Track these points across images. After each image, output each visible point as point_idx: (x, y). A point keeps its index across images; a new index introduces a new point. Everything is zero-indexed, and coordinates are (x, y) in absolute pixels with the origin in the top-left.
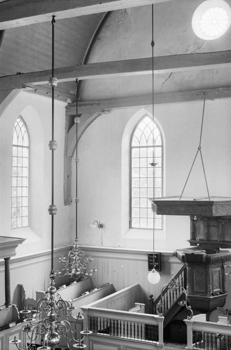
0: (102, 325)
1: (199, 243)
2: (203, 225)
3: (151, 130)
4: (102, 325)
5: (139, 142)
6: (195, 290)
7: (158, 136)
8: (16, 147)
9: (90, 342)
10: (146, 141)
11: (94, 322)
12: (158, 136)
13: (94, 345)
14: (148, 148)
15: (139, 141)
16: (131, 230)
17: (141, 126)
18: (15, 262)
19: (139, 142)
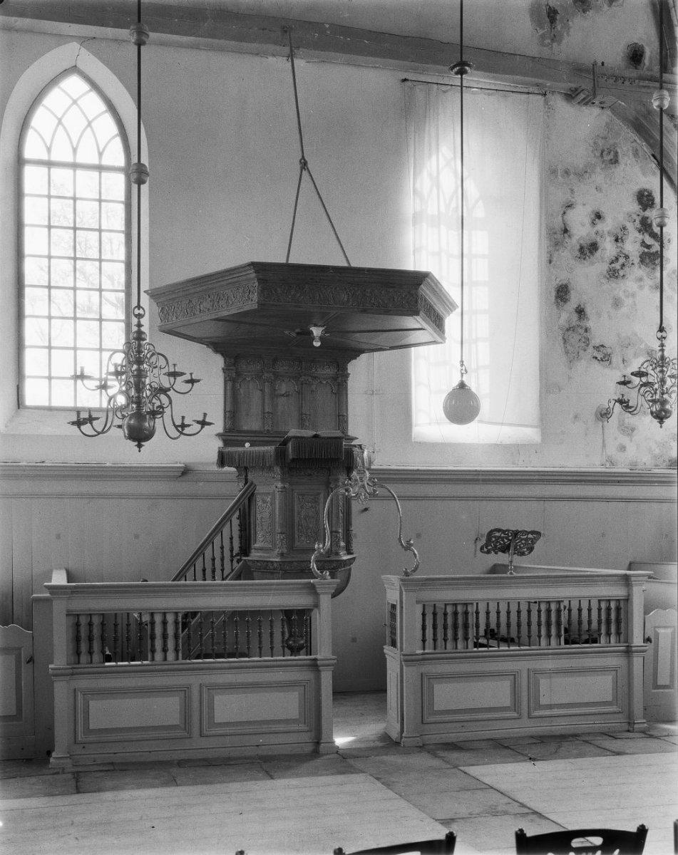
0: (266, 637)
1: (248, 441)
2: (259, 393)
3: (55, 116)
4: (266, 637)
5: (75, 150)
6: (297, 544)
7: (55, 131)
8: (69, 172)
9: (75, 697)
10: (71, 151)
11: (91, 647)
12: (55, 131)
13: (93, 704)
14: (104, 174)
15: (101, 150)
16: (22, 412)
17: (54, 99)
18: (609, 481)
19: (75, 150)
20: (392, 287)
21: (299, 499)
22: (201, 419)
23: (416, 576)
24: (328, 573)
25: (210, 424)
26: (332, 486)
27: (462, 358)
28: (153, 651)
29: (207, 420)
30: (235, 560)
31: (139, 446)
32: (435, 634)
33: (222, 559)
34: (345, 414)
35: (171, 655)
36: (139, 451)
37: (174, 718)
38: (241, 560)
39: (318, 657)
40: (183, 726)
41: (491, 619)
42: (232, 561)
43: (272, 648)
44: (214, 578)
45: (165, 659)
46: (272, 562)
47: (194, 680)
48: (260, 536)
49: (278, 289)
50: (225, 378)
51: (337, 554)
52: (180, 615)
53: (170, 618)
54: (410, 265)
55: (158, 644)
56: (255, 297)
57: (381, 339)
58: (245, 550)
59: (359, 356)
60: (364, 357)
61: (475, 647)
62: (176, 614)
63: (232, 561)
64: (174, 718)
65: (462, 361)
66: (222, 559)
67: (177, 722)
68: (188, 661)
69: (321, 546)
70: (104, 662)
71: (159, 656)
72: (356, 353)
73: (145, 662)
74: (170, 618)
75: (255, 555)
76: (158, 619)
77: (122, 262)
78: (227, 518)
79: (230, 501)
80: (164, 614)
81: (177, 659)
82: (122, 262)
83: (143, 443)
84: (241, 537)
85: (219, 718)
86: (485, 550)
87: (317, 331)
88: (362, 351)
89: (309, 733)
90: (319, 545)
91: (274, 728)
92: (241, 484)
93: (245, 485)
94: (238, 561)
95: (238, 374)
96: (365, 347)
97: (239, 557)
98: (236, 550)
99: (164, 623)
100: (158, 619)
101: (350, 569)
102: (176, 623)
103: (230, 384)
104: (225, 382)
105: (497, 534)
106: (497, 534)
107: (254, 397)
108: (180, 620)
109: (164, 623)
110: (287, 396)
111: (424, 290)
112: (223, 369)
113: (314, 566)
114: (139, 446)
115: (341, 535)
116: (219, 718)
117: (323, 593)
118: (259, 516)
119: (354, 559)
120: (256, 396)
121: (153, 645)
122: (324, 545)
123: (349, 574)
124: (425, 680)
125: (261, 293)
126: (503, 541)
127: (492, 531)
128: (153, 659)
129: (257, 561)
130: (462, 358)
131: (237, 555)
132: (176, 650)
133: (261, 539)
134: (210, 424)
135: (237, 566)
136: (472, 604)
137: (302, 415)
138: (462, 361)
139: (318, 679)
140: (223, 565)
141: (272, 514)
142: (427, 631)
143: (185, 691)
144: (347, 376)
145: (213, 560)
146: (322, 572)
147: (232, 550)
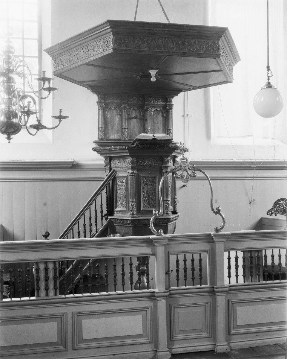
20: (202, 39)
21: (143, 180)
22: (58, 114)
23: (222, 232)
24: (162, 231)
25: (65, 117)
26: (164, 171)
27: (268, 64)
28: (38, 290)
29: (63, 114)
30: (104, 219)
31: (9, 138)
32: (237, 273)
33: (96, 218)
34: (171, 129)
35: (51, 293)
36: (9, 142)
37: (54, 337)
38: (108, 218)
39: (156, 290)
40: (60, 343)
41: (275, 261)
42: (102, 219)
43: (123, 285)
44: (85, 237)
45: (47, 295)
46: (127, 220)
47: (69, 310)
48: (119, 203)
49: (126, 40)
50: (98, 107)
51: (167, 214)
52: (57, 263)
53: (51, 266)
54: (212, 22)
55: (51, 275)
56: (111, 46)
57: (194, 80)
58: (111, 211)
59: (179, 93)
60: (181, 94)
61: (264, 280)
62: (54, 262)
63: (102, 219)
64: (54, 337)
65: (268, 67)
66: (96, 218)
67: (56, 340)
68: (63, 296)
69: (157, 212)
70: (2, 299)
71: (43, 293)
72: (177, 91)
73: (32, 298)
74: (51, 266)
75: (116, 216)
76: (42, 267)
77: (36, 39)
78: (99, 192)
79: (100, 182)
80: (46, 263)
81: (56, 294)
82: (36, 39)
83: (12, 136)
84: (107, 204)
85: (85, 336)
86: (270, 213)
87: (153, 73)
88: (181, 91)
89: (150, 345)
90: (155, 211)
91: (126, 341)
92: (108, 171)
93: (110, 171)
94: (106, 219)
95: (107, 105)
96: (181, 87)
97: (106, 217)
98: (105, 212)
99: (46, 269)
100: (42, 267)
101: (176, 222)
102: (55, 269)
103: (101, 112)
104: (99, 110)
105: (281, 202)
106: (281, 202)
107: (115, 117)
108: (58, 267)
109: (46, 269)
110: (136, 118)
111: (227, 31)
112: (97, 102)
113: (152, 227)
114: (9, 138)
115: (170, 202)
116: (85, 336)
117: (159, 246)
118: (119, 192)
119: (178, 216)
120: (117, 118)
121: (38, 286)
122: (159, 212)
123: (175, 226)
124: (231, 304)
125: (115, 42)
126: (283, 206)
127: (279, 200)
128: (38, 295)
129: (118, 219)
130: (268, 64)
131: (105, 215)
132: (55, 289)
133: (120, 205)
134: (65, 117)
135: (105, 222)
136: (262, 251)
137: (145, 129)
138: (268, 67)
139: (155, 307)
140: (96, 222)
141: (127, 189)
142: (231, 270)
143: (60, 318)
144: (171, 106)
145: (90, 219)
146: (158, 231)
147: (102, 212)
